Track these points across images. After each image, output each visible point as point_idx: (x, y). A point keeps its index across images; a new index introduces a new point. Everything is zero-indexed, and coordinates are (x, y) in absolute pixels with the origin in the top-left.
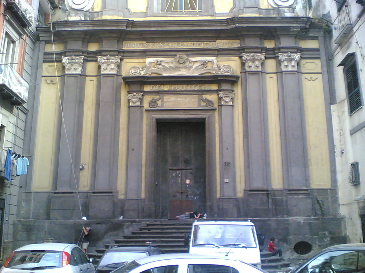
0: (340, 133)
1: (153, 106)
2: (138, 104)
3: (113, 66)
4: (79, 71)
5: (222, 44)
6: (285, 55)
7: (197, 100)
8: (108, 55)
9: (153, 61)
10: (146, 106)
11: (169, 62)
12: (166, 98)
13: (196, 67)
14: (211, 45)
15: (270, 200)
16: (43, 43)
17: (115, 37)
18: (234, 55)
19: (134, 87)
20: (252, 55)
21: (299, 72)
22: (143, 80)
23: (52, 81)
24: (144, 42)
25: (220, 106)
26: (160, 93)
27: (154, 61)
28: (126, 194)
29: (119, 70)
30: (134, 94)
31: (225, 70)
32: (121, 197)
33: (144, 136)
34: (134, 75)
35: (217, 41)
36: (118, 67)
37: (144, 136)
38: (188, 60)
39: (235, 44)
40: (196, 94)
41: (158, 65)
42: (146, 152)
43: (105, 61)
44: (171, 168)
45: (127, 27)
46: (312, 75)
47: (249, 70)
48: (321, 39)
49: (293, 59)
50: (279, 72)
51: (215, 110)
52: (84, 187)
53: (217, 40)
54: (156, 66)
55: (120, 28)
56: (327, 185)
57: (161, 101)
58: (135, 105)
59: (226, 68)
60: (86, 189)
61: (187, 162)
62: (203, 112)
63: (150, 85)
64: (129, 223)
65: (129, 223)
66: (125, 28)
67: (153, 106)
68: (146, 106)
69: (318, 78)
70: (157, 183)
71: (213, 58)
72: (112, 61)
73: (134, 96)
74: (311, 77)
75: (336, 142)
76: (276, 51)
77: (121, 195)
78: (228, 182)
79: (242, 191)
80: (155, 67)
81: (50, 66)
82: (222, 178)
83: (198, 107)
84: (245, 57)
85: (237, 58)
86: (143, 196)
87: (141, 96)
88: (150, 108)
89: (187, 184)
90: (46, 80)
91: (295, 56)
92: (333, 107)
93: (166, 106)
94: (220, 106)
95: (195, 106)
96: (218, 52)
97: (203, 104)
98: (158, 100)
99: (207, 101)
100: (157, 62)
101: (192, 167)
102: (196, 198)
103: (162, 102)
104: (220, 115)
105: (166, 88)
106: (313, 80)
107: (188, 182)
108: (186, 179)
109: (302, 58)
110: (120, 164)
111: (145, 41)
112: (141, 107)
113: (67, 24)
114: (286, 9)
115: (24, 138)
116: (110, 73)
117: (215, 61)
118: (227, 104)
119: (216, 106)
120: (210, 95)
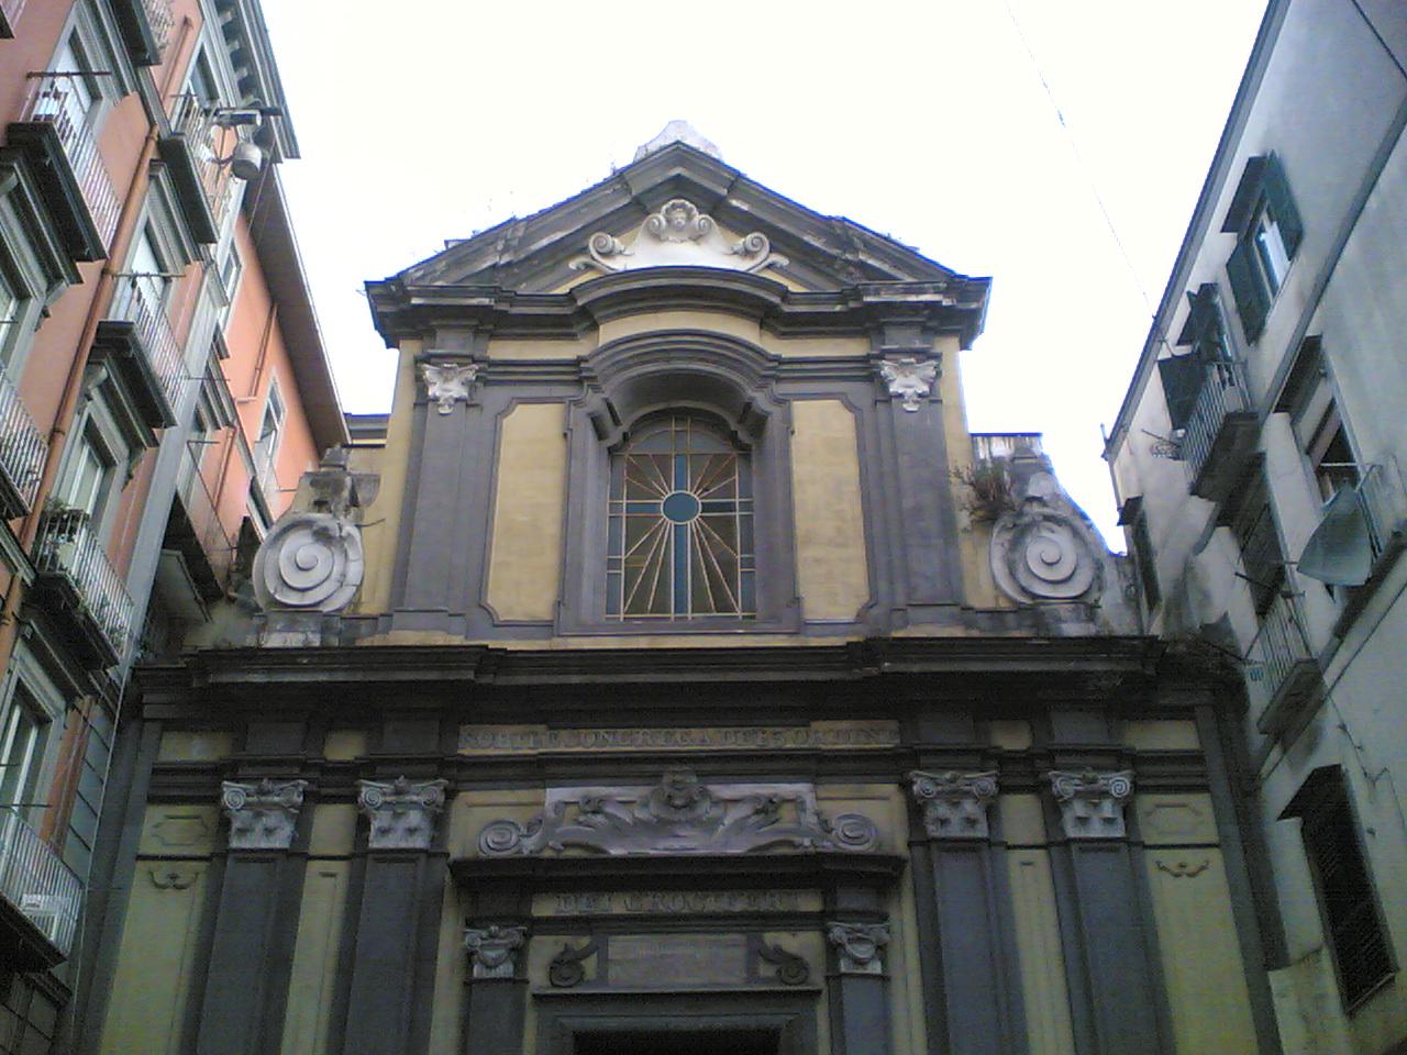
2: (505, 970)
3: (415, 818)
4: (281, 841)
5: (831, 735)
7: (740, 953)
10: (538, 977)
12: (619, 946)
14: (790, 739)
18: (883, 776)
20: (948, 775)
35: (815, 725)
38: (705, 794)
39: (884, 737)
49: (1105, 794)
50: (1056, 844)
58: (493, 974)
66: (470, 675)
68: (538, 977)
73: (492, 936)
83: (748, 982)
87: (518, 939)
95: (735, 981)
96: (818, 766)
97: (766, 971)
98: (585, 954)
99: (779, 957)
103: (604, 961)
105: (618, 905)
106: (1192, 875)
112: (518, 981)
117: (809, 799)
118: (860, 971)
119: (817, 980)
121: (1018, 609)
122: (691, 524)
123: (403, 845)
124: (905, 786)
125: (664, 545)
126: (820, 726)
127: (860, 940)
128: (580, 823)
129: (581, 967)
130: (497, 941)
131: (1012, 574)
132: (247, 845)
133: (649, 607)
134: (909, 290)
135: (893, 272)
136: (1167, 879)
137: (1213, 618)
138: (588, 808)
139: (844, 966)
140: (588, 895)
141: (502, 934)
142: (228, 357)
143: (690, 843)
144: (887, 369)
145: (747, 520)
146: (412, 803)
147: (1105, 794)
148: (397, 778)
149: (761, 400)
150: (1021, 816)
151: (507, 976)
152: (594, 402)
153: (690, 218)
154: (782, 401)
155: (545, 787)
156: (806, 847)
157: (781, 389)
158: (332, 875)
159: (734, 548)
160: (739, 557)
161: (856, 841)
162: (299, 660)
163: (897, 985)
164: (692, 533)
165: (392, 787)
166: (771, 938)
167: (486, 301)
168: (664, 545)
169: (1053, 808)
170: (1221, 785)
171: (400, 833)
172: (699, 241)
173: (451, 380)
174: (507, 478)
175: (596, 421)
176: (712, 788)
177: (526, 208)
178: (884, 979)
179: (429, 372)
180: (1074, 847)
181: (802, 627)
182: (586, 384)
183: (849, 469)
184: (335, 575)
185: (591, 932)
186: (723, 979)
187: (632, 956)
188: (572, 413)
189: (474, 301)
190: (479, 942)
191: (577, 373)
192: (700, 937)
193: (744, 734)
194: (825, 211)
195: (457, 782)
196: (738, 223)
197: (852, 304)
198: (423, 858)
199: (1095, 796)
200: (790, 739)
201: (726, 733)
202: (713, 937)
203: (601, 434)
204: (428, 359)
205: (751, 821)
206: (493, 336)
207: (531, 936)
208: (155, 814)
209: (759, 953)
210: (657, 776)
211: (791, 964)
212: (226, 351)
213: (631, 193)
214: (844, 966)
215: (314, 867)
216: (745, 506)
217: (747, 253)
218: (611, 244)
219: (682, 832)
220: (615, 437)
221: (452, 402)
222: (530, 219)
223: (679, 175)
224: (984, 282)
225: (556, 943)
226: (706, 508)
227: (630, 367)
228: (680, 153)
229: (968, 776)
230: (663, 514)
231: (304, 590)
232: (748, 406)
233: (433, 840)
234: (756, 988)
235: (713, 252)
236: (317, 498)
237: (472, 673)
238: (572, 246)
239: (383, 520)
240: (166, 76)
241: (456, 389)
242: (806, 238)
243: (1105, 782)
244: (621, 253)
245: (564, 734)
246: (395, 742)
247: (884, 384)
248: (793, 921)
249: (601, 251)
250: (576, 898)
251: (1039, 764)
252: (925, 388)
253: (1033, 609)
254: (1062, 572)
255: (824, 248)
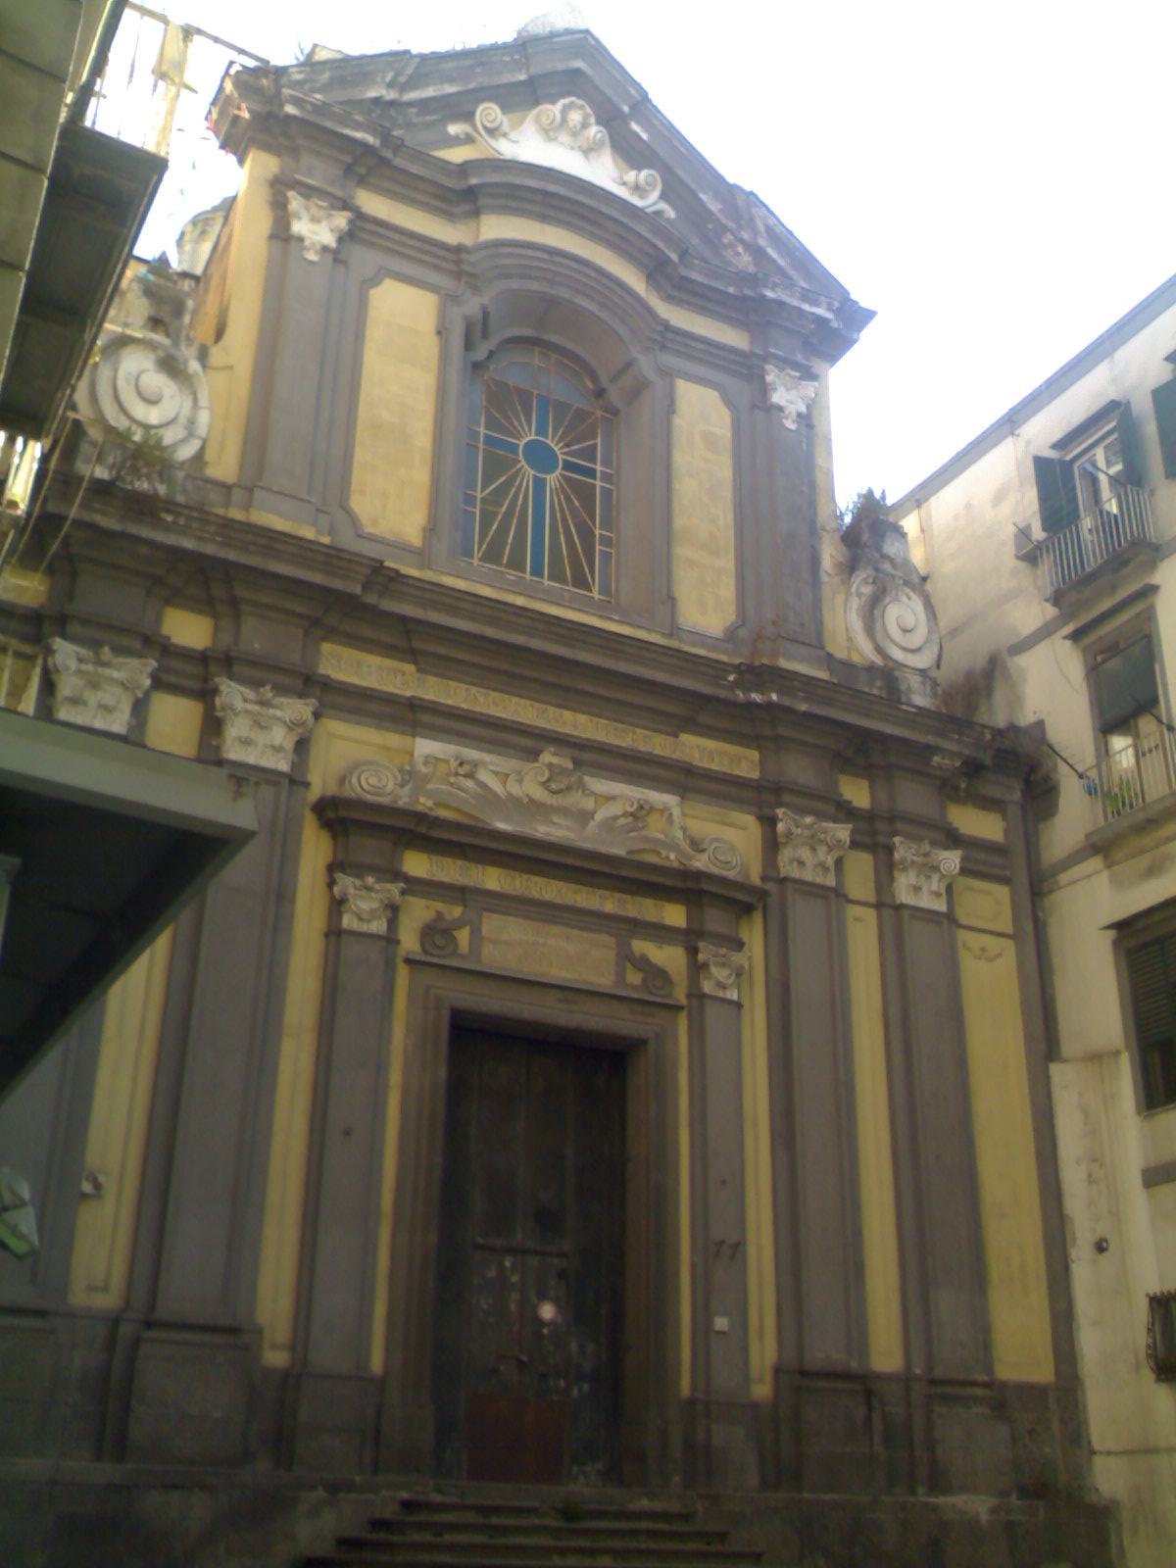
0: (1090, 1176)
1: (438, 947)
2: (378, 926)
3: (279, 735)
5: (698, 749)
7: (611, 955)
8: (268, 687)
9: (442, 757)
10: (409, 941)
12: (492, 924)
13: (608, 819)
14: (658, 744)
17: (299, 615)
18: (740, 802)
19: (368, 848)
20: (808, 820)
21: (950, 918)
22: (411, 825)
24: (410, 668)
25: (697, 996)
27: (446, 758)
28: (300, 1343)
30: (370, 880)
32: (276, 1358)
33: (395, 1076)
34: (369, 798)
35: (684, 737)
37: (395, 1076)
39: (743, 762)
42: (402, 1150)
43: (250, 707)
44: (480, 1240)
45: (364, 588)
46: (987, 939)
48: (1014, 810)
50: (884, 903)
51: (678, 1008)
52: (91, 1289)
54: (452, 780)
55: (337, 584)
56: (1043, 1372)
58: (364, 928)
60: (108, 1301)
61: (548, 1221)
64: (320, 1493)
65: (320, 1493)
66: (357, 590)
67: (438, 947)
68: (409, 941)
75: (1076, 1203)
76: (880, 825)
77: (275, 1347)
79: (768, 1376)
80: (452, 785)
85: (749, 820)
86: (377, 1363)
89: (541, 1323)
92: (1055, 1069)
95: (604, 981)
96: (686, 780)
97: (634, 977)
98: (459, 924)
99: (643, 964)
100: (461, 764)
102: (580, 1390)
103: (476, 933)
105: (492, 879)
106: (991, 960)
107: (547, 1311)
108: (542, 1296)
109: (965, 871)
110: (273, 1197)
112: (391, 940)
114: (915, 681)
116: (264, 763)
117: (676, 811)
119: (680, 995)
120: (660, 947)
121: (871, 669)
122: (552, 479)
124: (769, 822)
125: (521, 496)
126: (688, 739)
127: (724, 965)
128: (452, 785)
129: (454, 938)
131: (870, 630)
133: (505, 561)
134: (805, 298)
135: (792, 273)
137: (1026, 718)
139: (707, 987)
144: (772, 375)
145: (607, 494)
147: (935, 868)
148: (263, 686)
149: (645, 364)
150: (860, 875)
151: (380, 933)
153: (585, 125)
154: (669, 375)
155: (414, 736)
156: (671, 861)
157: (669, 360)
159: (593, 518)
160: (597, 532)
164: (551, 490)
166: (642, 947)
167: (370, 139)
168: (521, 496)
169: (886, 870)
170: (1022, 881)
172: (593, 155)
174: (374, 361)
177: (422, 43)
178: (738, 1005)
179: (295, 202)
180: (906, 913)
181: (674, 631)
182: (464, 280)
183: (725, 471)
185: (464, 903)
188: (554, 338)
189: (358, 135)
192: (575, 932)
194: (731, 179)
196: (630, 152)
197: (747, 292)
198: (286, 782)
200: (658, 744)
202: (591, 935)
203: (468, 345)
204: (295, 185)
205: (622, 821)
209: (626, 957)
210: (533, 755)
211: (657, 975)
213: (528, 70)
216: (607, 477)
217: (637, 188)
218: (499, 120)
219: (556, 819)
220: (481, 353)
222: (423, 58)
223: (578, 72)
224: (870, 315)
225: (428, 907)
226: (568, 466)
228: (584, 44)
230: (521, 458)
232: (629, 365)
233: (294, 766)
234: (623, 993)
235: (602, 172)
236: (152, 313)
238: (460, 108)
239: (231, 368)
242: (703, 197)
244: (505, 135)
245: (432, 680)
246: (256, 637)
247: (764, 389)
248: (660, 932)
249: (488, 125)
250: (484, 868)
251: (880, 825)
252: (803, 409)
253: (888, 675)
255: (719, 215)
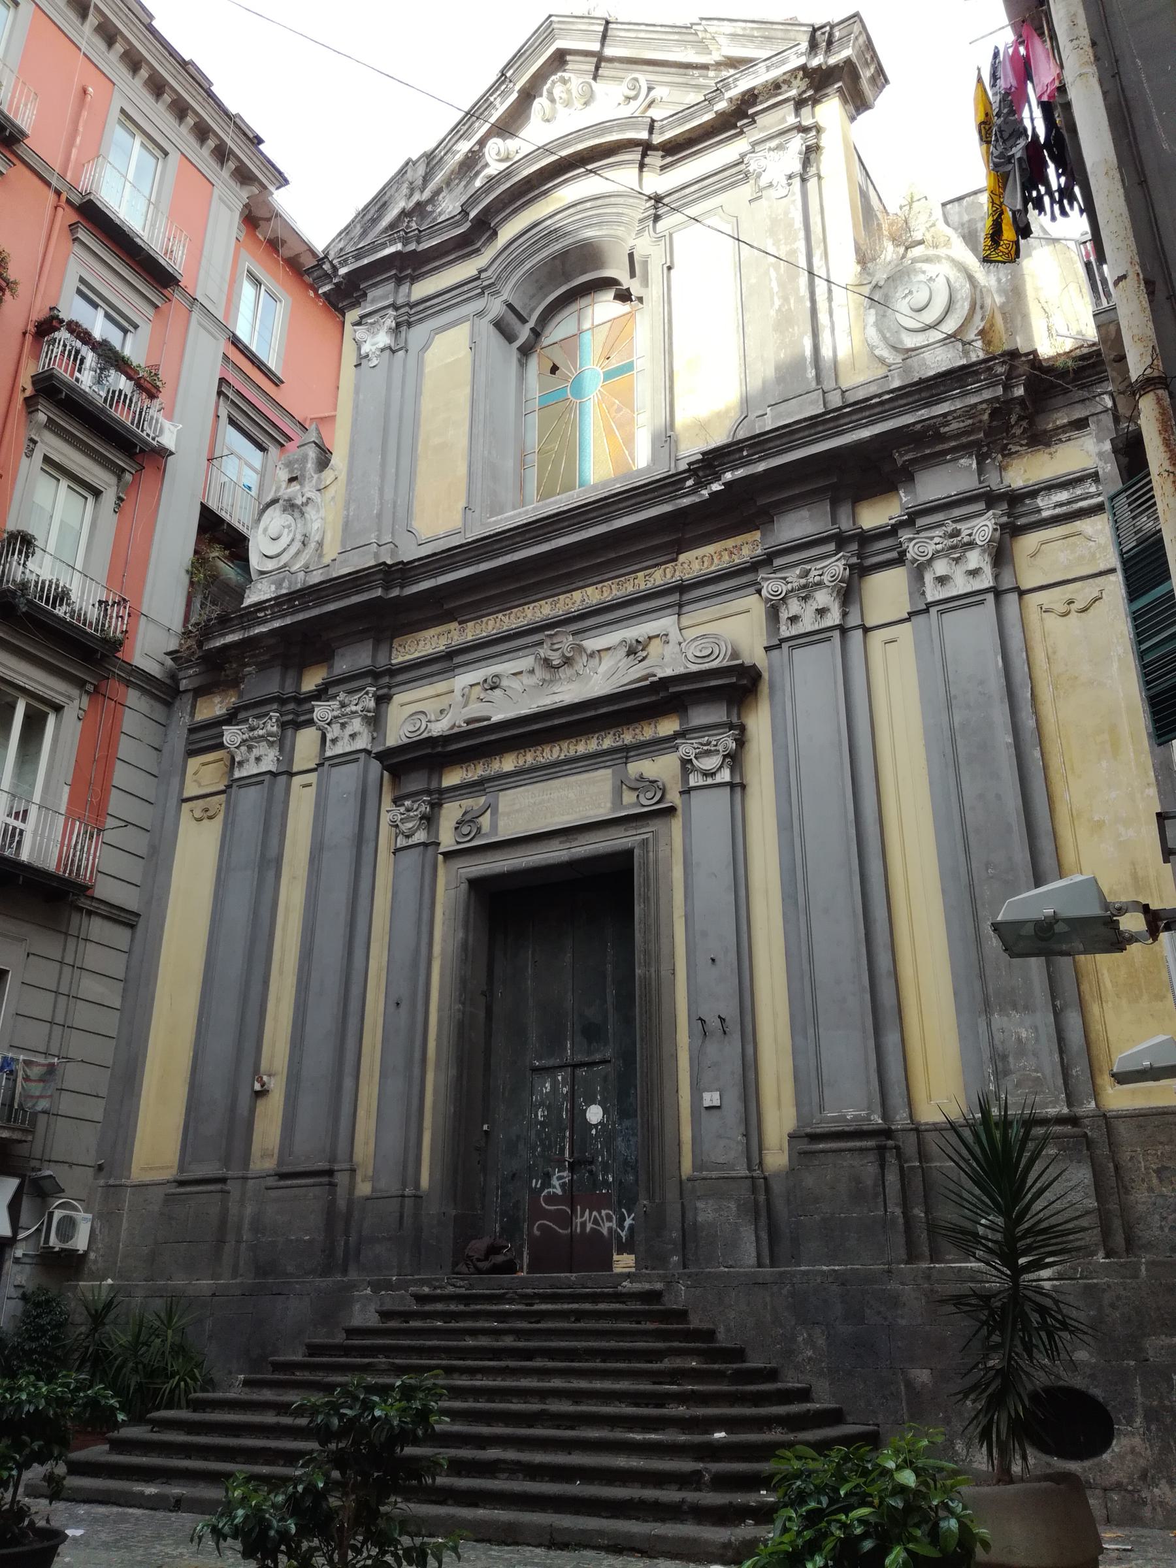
4: (269, 763)
6: (932, 538)
11: (521, 673)
15: (892, 1178)
16: (188, 698)
23: (207, 810)
26: (486, 785)
29: (375, 735)
31: (698, 654)
35: (682, 557)
36: (375, 725)
38: (580, 649)
40: (602, 765)
41: (489, 692)
47: (794, 631)
49: (971, 545)
51: (671, 810)
53: (679, 552)
57: (492, 814)
58: (411, 842)
59: (700, 647)
62: (626, 830)
63: (459, 766)
66: (379, 592)
68: (447, 839)
69: (1104, 595)
70: (485, 1127)
71: (666, 623)
72: (354, 708)
73: (408, 810)
74: (1068, 596)
78: (717, 1103)
81: (203, 764)
82: (697, 1090)
83: (614, 809)
84: (772, 586)
87: (425, 808)
88: (458, 843)
90: (192, 811)
91: (975, 531)
93: (509, 828)
94: (687, 791)
95: (603, 810)
97: (629, 797)
99: (644, 784)
101: (608, 1054)
104: (687, 829)
111: (456, 620)
113: (228, 624)
115: (122, 1005)
118: (710, 781)
123: (348, 749)
127: (708, 753)
130: (412, 814)
132: (245, 774)
136: (1051, 621)
138: (486, 686)
140: (483, 760)
141: (415, 806)
142: (282, 382)
143: (568, 692)
146: (353, 713)
152: (496, 307)
158: (310, 785)
161: (707, 660)
162: (259, 615)
163: (753, 789)
165: (338, 703)
171: (347, 737)
173: (377, 333)
175: (499, 325)
176: (585, 643)
184: (299, 537)
186: (591, 813)
187: (517, 807)
190: (400, 817)
191: (479, 286)
193: (618, 584)
195: (390, 688)
199: (959, 549)
201: (602, 588)
203: (510, 337)
206: (414, 279)
207: (441, 805)
208: (194, 763)
212: (278, 378)
214: (694, 780)
215: (297, 781)
220: (524, 333)
221: (378, 353)
227: (522, 262)
229: (818, 567)
231: (278, 555)
237: (380, 589)
240: (1155, 239)
241: (383, 339)
243: (969, 531)
254: (930, 317)
